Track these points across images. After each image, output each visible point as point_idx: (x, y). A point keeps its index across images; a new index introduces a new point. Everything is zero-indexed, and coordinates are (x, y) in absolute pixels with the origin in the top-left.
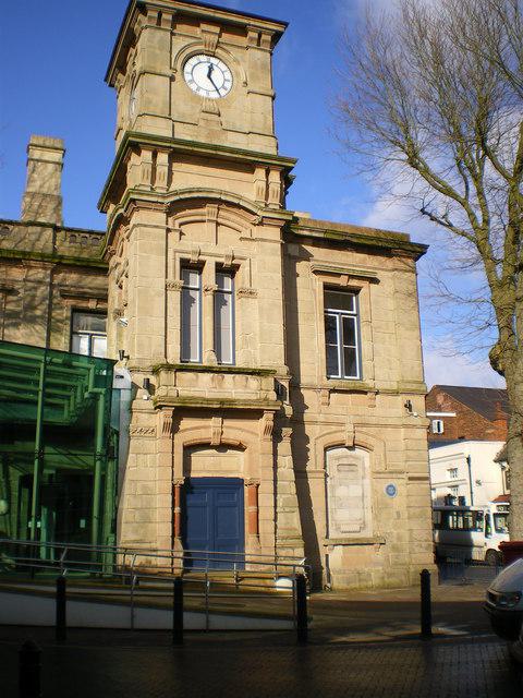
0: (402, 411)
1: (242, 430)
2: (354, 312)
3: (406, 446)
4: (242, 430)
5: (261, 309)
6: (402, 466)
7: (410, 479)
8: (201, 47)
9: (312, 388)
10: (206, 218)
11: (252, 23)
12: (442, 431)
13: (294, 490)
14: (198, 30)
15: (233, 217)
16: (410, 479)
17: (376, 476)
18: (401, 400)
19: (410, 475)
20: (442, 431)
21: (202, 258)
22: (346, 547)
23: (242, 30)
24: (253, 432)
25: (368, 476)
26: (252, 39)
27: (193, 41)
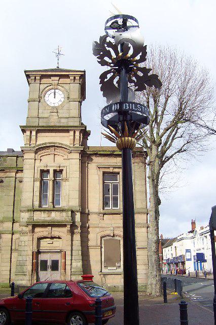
21: (48, 168)
24: (63, 232)
26: (71, 80)
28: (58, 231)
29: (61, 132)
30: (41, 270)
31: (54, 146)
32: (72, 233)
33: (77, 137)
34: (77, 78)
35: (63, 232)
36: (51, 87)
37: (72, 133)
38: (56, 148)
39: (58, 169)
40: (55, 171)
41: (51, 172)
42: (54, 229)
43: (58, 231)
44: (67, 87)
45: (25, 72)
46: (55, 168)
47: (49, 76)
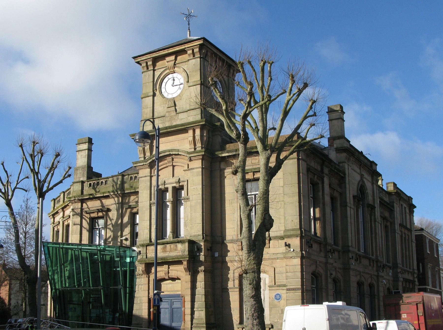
0: (283, 249)
1: (177, 271)
2: (254, 196)
3: (286, 270)
4: (177, 271)
5: (191, 206)
6: (284, 282)
7: (288, 290)
8: (168, 71)
9: (232, 241)
10: (168, 165)
11: (186, 46)
12: (67, 285)
13: (204, 299)
14: (165, 61)
15: (181, 160)
16: (288, 290)
17: (271, 288)
18: (282, 242)
19: (288, 287)
20: (67, 285)
21: (166, 186)
22: (418, 325)
23: (183, 52)
24: (179, 271)
25: (267, 288)
26: (189, 55)
27: (164, 69)
28: (176, 270)
29: (169, 136)
30: (328, 306)
31: (170, 155)
32: (193, 272)
33: (198, 137)
34: (196, 50)
35: (179, 271)
36: (168, 71)
37: (191, 132)
38: (174, 156)
39: (177, 185)
40: (174, 188)
41: (170, 190)
42: (172, 267)
43: (176, 270)
44: (185, 66)
45: (134, 58)
46: (174, 185)
47: (163, 57)
